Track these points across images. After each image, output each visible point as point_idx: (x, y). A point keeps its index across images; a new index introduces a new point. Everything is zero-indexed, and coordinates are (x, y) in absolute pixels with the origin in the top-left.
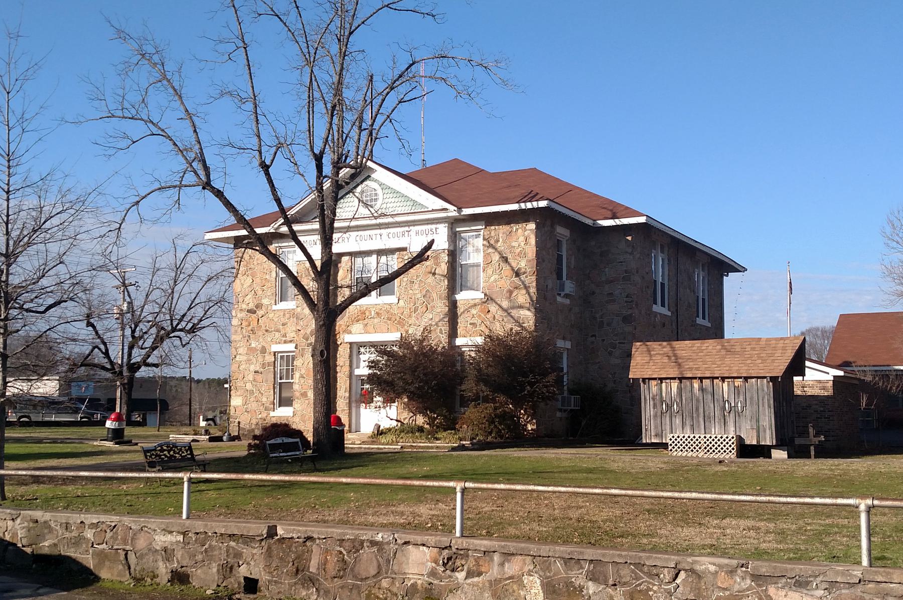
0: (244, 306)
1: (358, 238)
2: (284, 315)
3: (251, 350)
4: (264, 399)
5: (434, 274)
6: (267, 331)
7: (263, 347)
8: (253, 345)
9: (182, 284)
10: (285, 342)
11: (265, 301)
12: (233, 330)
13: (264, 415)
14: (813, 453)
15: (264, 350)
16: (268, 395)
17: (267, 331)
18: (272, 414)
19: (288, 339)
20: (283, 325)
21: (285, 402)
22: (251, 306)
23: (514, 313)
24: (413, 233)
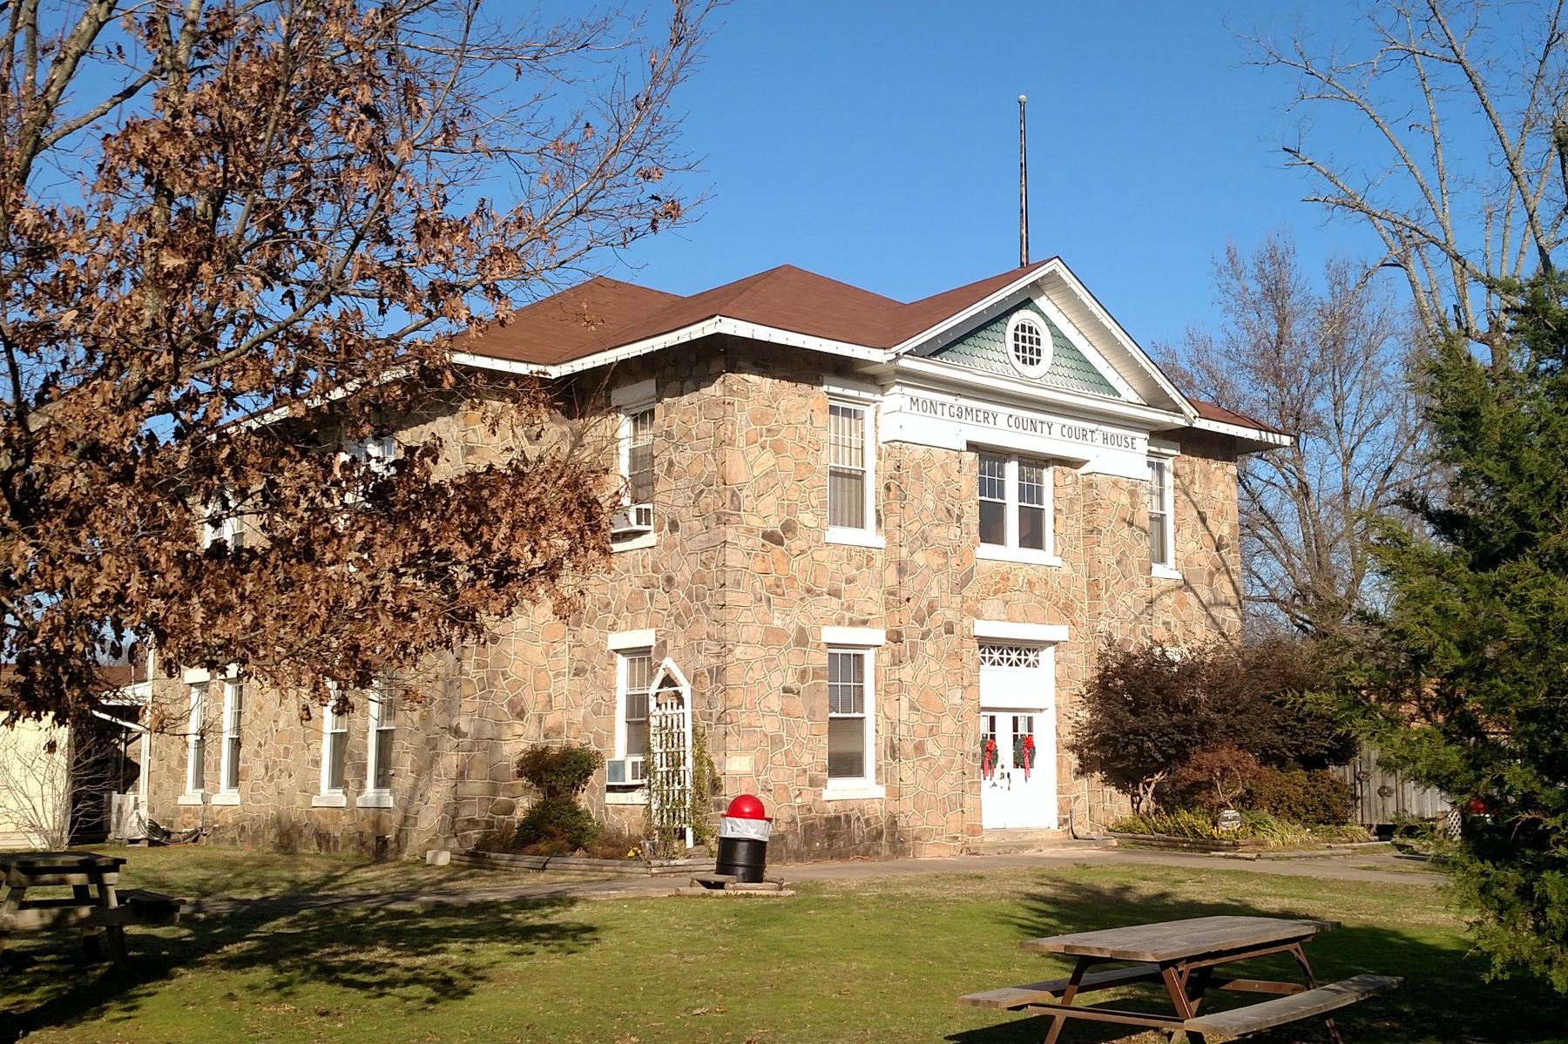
0: (755, 522)
1: (1012, 421)
2: (850, 558)
3: (773, 636)
4: (806, 759)
5: (1131, 524)
6: (809, 591)
7: (801, 630)
8: (777, 623)
9: (567, 208)
10: (852, 623)
11: (806, 518)
12: (467, 690)
13: (808, 797)
14: (857, 715)
15: (802, 639)
16: (818, 752)
17: (809, 591)
18: (827, 794)
19: (857, 616)
20: (849, 581)
21: (846, 764)
22: (774, 524)
23: (1214, 612)
24: (1098, 436)
